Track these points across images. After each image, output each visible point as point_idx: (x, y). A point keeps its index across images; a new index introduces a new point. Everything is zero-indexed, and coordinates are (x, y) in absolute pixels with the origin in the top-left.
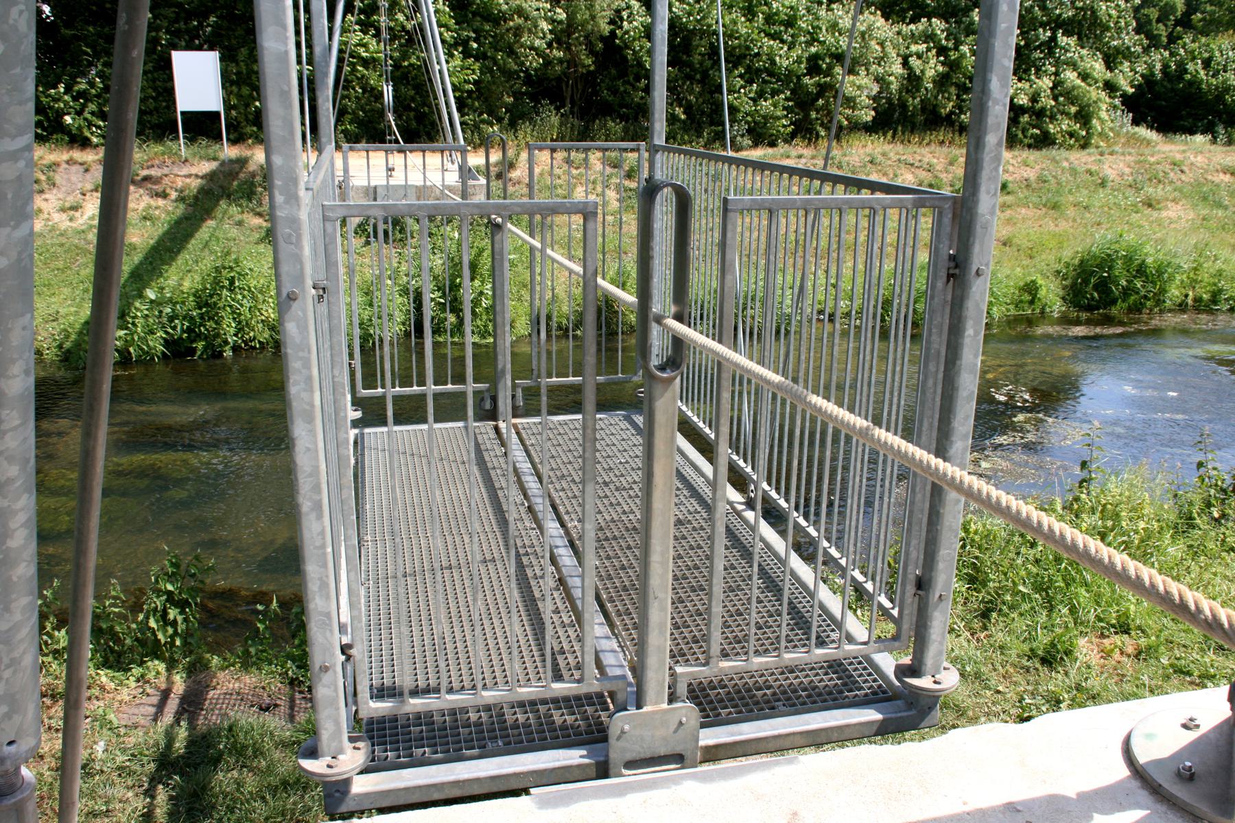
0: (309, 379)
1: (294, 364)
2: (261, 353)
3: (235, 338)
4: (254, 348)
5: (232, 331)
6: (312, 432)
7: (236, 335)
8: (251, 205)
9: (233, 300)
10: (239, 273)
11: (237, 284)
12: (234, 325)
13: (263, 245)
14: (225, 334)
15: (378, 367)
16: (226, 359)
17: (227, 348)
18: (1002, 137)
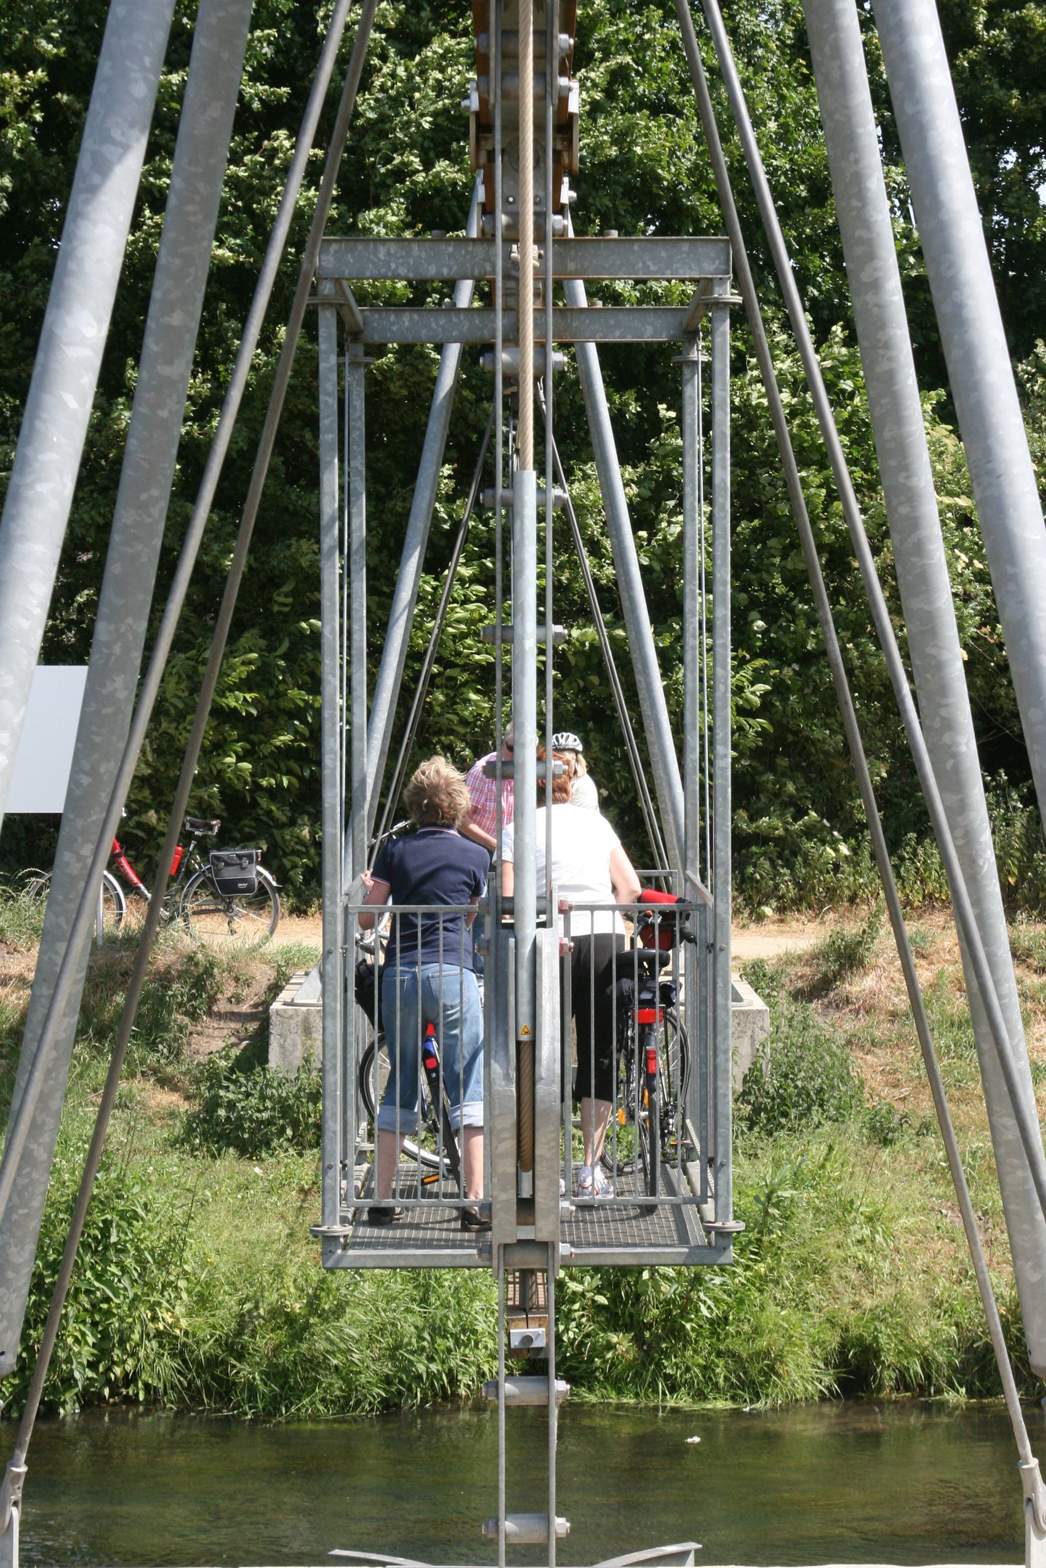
0: (335, 996)
1: (412, 520)
2: (147, 1412)
3: (90, 1374)
4: (131, 1401)
5: (87, 1353)
6: (335, 1025)
7: (92, 1365)
8: (152, 1058)
9: (99, 1277)
10: (122, 1215)
11: (113, 1239)
12: (91, 1340)
13: (175, 1157)
14: (68, 1360)
15: (376, 992)
16: (63, 1422)
17: (69, 1396)
18: (613, 860)
